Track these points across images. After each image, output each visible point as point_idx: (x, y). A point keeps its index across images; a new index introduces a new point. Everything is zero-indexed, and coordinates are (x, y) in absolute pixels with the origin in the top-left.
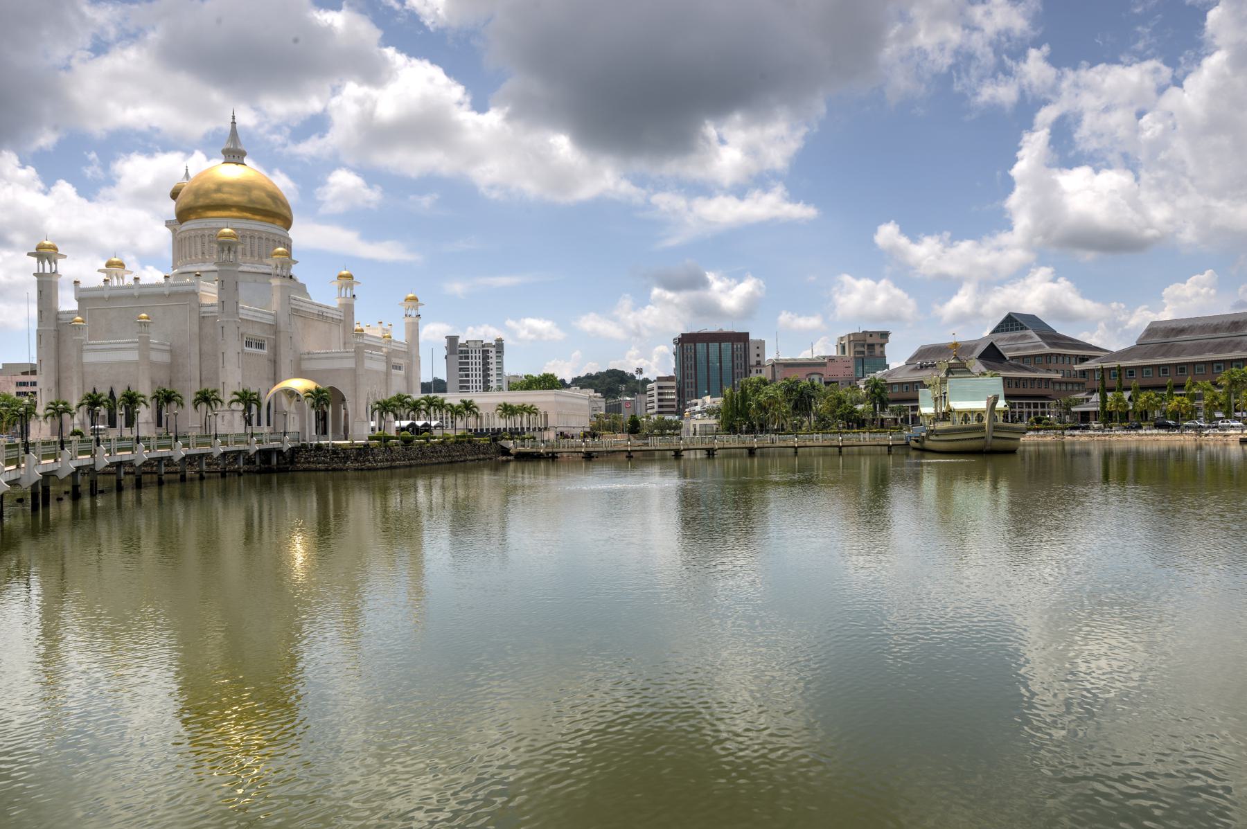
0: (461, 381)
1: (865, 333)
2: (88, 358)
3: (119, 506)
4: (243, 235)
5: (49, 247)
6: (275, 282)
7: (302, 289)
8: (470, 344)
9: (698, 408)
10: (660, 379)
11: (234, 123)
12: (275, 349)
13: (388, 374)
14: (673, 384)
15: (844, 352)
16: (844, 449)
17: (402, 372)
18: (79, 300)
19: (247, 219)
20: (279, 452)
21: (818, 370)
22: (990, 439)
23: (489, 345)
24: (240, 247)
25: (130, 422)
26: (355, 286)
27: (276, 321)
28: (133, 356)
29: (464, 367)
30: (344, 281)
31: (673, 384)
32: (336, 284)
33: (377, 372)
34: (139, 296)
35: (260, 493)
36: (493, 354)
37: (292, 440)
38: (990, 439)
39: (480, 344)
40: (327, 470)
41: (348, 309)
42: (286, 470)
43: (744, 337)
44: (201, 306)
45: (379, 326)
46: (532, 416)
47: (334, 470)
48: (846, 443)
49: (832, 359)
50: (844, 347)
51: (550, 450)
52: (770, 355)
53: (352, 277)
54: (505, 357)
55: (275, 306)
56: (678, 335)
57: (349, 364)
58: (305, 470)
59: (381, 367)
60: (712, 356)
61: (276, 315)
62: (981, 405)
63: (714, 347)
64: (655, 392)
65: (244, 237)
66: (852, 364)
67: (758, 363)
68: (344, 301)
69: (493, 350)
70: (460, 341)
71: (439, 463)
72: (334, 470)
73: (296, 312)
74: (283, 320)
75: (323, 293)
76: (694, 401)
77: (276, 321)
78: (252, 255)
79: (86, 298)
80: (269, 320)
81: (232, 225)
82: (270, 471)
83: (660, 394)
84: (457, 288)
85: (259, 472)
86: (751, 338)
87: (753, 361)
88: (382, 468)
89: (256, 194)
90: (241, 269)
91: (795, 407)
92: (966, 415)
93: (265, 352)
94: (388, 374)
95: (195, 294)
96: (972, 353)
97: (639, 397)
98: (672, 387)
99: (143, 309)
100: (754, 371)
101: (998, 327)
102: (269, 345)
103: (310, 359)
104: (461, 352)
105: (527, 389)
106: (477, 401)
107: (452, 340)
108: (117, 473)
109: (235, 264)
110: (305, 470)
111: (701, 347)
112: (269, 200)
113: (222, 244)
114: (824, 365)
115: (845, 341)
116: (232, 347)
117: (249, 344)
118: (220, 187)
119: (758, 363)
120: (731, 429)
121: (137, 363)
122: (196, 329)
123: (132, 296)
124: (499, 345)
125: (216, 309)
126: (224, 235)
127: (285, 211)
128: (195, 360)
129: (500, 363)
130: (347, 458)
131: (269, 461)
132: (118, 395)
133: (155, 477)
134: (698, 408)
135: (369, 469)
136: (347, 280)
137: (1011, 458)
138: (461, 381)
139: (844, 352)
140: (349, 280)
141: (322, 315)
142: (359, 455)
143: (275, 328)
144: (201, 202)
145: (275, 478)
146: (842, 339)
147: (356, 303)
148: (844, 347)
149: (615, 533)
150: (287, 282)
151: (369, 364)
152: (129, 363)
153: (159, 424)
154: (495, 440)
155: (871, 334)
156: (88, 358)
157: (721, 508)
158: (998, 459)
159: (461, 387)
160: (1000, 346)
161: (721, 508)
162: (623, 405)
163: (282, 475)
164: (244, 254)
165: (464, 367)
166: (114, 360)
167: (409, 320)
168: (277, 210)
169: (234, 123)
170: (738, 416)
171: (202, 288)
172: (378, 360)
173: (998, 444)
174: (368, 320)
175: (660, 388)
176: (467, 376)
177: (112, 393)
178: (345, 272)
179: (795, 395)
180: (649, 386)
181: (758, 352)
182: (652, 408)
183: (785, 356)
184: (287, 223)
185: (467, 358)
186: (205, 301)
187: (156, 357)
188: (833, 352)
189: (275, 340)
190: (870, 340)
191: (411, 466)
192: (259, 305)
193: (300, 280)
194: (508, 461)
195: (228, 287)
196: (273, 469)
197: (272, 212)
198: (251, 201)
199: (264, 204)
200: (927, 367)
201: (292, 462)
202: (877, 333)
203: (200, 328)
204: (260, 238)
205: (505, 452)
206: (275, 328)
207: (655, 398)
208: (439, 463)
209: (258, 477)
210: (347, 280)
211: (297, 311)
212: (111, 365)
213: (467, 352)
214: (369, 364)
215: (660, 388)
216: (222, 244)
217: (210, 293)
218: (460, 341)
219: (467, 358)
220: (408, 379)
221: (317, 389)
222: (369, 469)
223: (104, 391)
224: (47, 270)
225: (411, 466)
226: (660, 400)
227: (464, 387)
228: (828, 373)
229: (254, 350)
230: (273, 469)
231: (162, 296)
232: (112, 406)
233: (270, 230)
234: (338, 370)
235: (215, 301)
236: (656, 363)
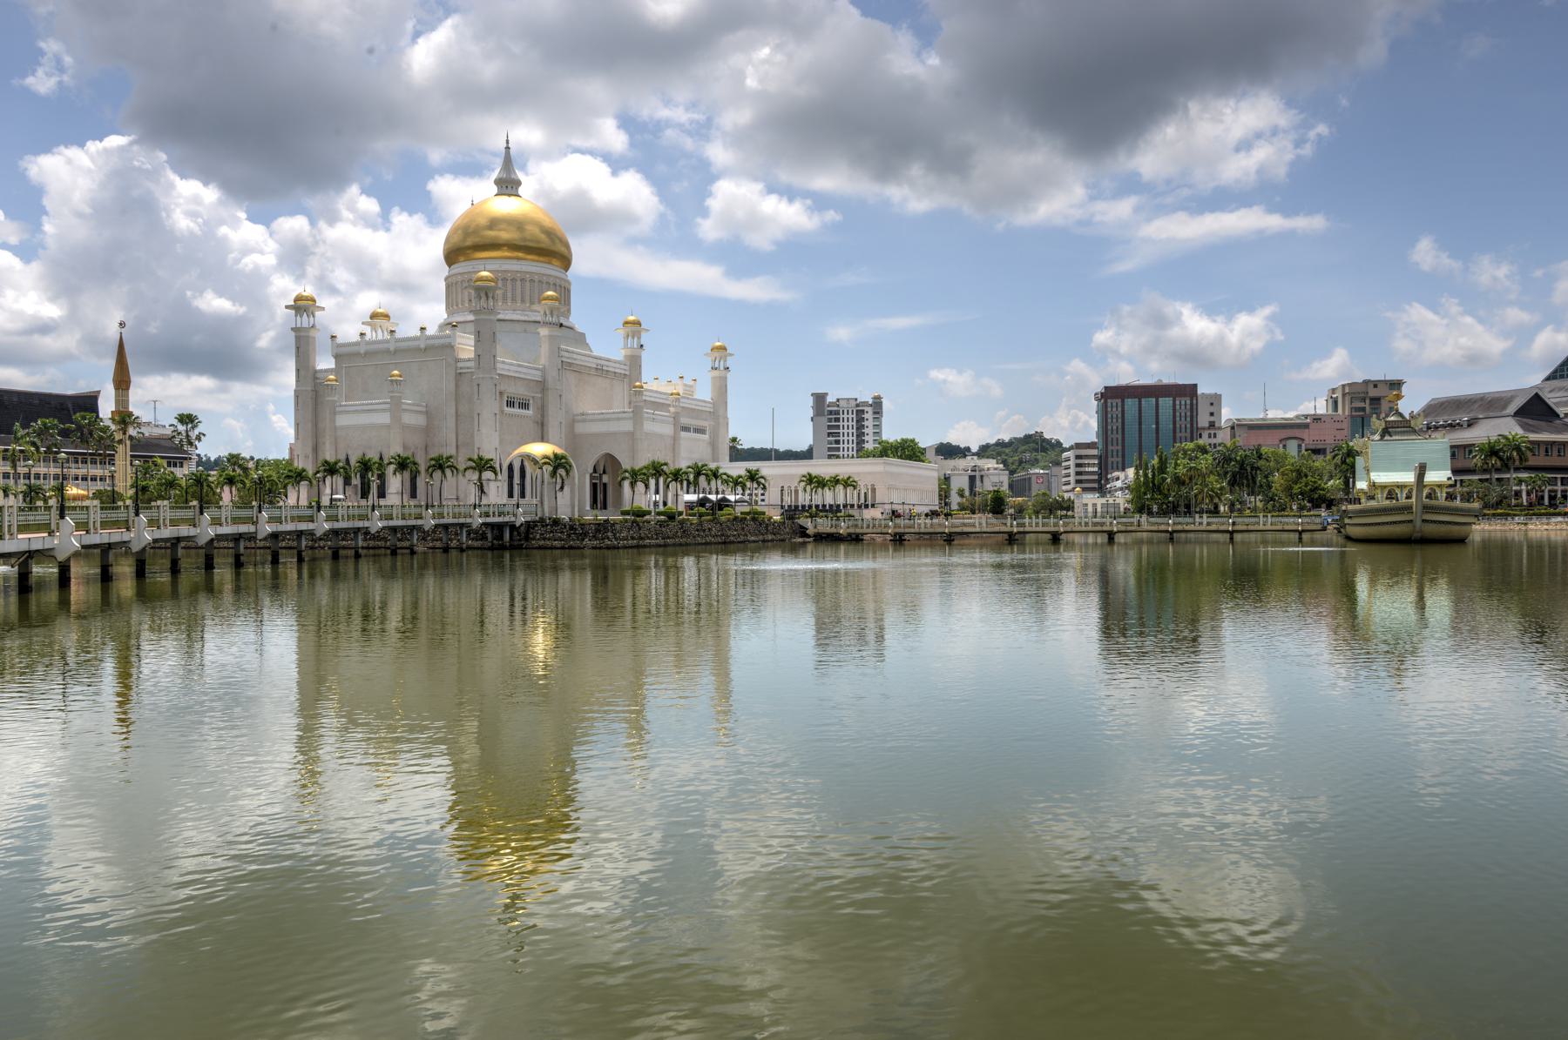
0: (830, 449)
1: (1366, 382)
2: (342, 421)
3: (275, 576)
4: (502, 278)
5: (307, 299)
6: (544, 331)
7: (580, 339)
8: (842, 403)
9: (1119, 484)
10: (1078, 446)
11: (508, 148)
12: (542, 410)
13: (675, 439)
14: (1095, 452)
15: (1336, 409)
16: (1238, 537)
17: (706, 437)
18: (337, 357)
19: (518, 259)
20: (513, 527)
21: (1297, 433)
22: (1418, 523)
23: (865, 404)
24: (499, 292)
25: (382, 494)
26: (643, 335)
27: (544, 377)
28: (385, 419)
29: (833, 431)
30: (630, 328)
31: (1095, 452)
32: (622, 332)
33: (661, 436)
34: (396, 351)
35: (485, 570)
36: (869, 416)
37: (525, 513)
38: (1418, 523)
39: (853, 403)
40: (563, 548)
41: (634, 362)
42: (520, 547)
43: (1190, 391)
44: (458, 360)
45: (679, 382)
46: (849, 490)
47: (571, 548)
48: (1179, 527)
49: (1317, 419)
50: (1336, 402)
51: (851, 530)
52: (1227, 414)
53: (639, 323)
54: (884, 420)
55: (543, 361)
56: (1100, 389)
57: (627, 426)
58: (540, 548)
59: (668, 430)
60: (1150, 421)
61: (543, 370)
62: (1409, 477)
63: (1148, 403)
64: (1072, 463)
65: (504, 280)
66: (1346, 425)
67: (1212, 425)
68: (629, 352)
69: (870, 409)
70: (830, 399)
71: (706, 544)
72: (571, 548)
73: (566, 366)
74: (552, 374)
75: (607, 345)
76: (1116, 474)
77: (544, 377)
78: (523, 301)
79: (345, 355)
80: (537, 376)
81: (510, 266)
82: (503, 548)
83: (1078, 465)
84: (841, 333)
85: (492, 548)
86: (1200, 391)
87: (1203, 421)
88: (625, 547)
89: (533, 230)
90: (500, 317)
91: (1232, 483)
92: (1390, 493)
93: (530, 412)
94: (675, 439)
95: (451, 347)
96: (1504, 407)
97: (1055, 470)
98: (1093, 457)
99: (396, 366)
100: (1205, 434)
101: (1555, 371)
102: (531, 404)
103: (584, 421)
104: (831, 413)
105: (881, 456)
106: (764, 472)
107: (819, 399)
108: (236, 547)
109: (492, 311)
110: (540, 548)
111: (1131, 403)
112: (543, 237)
113: (478, 289)
114: (1306, 426)
115: (1338, 395)
116: (489, 407)
117: (510, 404)
118: (494, 223)
119: (1212, 425)
120: (1142, 509)
121: (388, 427)
122: (452, 386)
123: (388, 351)
124: (877, 405)
125: (472, 364)
126: (481, 279)
127: (560, 248)
128: (451, 422)
129: (878, 426)
130: (585, 534)
131: (501, 537)
132: (353, 462)
133: (352, 552)
134: (1119, 484)
135: (608, 548)
136: (634, 328)
137: (1455, 549)
138: (830, 449)
139: (1336, 409)
140: (636, 328)
141: (601, 370)
142: (598, 531)
143: (542, 385)
144: (469, 242)
145: (507, 555)
146: (1333, 391)
147: (644, 355)
148: (1336, 402)
149: (990, 644)
150: (557, 332)
151: (649, 426)
152: (382, 426)
153: (413, 495)
154: (791, 518)
155: (1375, 384)
156: (342, 421)
157: (1155, 611)
158: (1433, 551)
159: (830, 457)
160: (1551, 399)
161: (1155, 611)
162: (1034, 479)
163: (515, 552)
164: (505, 299)
165: (833, 431)
166: (367, 425)
167: (716, 373)
168: (553, 248)
169: (508, 148)
170: (1158, 496)
171: (459, 340)
172: (662, 422)
173: (1431, 530)
174: (657, 379)
175: (1078, 457)
176: (837, 442)
177: (347, 460)
178: (631, 318)
179: (1233, 467)
180: (1065, 455)
181: (1212, 409)
182: (1068, 483)
183: (1253, 414)
184: (566, 261)
185: (837, 420)
186: (463, 355)
187: (409, 419)
188: (1321, 408)
189: (542, 399)
190: (1373, 393)
191: (665, 546)
192: (518, 360)
193: (579, 328)
194: (804, 544)
195: (485, 339)
196: (510, 545)
197: (548, 249)
198: (525, 240)
199: (538, 242)
200: (1436, 428)
201: (527, 538)
202: (1385, 382)
203: (457, 386)
204: (532, 281)
205: (803, 532)
206: (542, 385)
207: (1072, 471)
208: (706, 544)
209: (489, 554)
210: (634, 328)
211: (570, 364)
212: (363, 428)
213: (837, 413)
214: (649, 426)
215: (1078, 457)
216: (478, 289)
217: (466, 346)
218: (830, 399)
219: (837, 420)
220: (713, 444)
221: (556, 455)
222: (608, 548)
223: (373, 455)
224: (305, 325)
225: (665, 546)
226: (1078, 473)
227: (833, 454)
228: (1310, 438)
229: (516, 411)
230: (510, 545)
231: (418, 349)
232: (366, 475)
233: (543, 271)
234: (614, 434)
235: (472, 355)
236: (1076, 424)
